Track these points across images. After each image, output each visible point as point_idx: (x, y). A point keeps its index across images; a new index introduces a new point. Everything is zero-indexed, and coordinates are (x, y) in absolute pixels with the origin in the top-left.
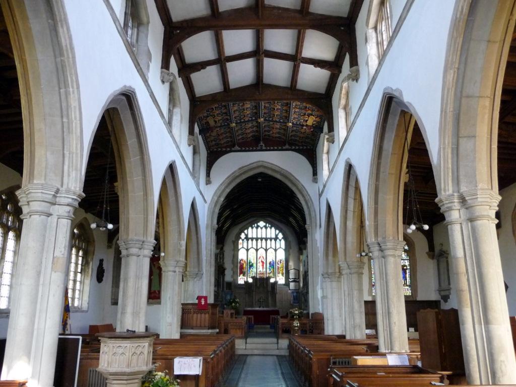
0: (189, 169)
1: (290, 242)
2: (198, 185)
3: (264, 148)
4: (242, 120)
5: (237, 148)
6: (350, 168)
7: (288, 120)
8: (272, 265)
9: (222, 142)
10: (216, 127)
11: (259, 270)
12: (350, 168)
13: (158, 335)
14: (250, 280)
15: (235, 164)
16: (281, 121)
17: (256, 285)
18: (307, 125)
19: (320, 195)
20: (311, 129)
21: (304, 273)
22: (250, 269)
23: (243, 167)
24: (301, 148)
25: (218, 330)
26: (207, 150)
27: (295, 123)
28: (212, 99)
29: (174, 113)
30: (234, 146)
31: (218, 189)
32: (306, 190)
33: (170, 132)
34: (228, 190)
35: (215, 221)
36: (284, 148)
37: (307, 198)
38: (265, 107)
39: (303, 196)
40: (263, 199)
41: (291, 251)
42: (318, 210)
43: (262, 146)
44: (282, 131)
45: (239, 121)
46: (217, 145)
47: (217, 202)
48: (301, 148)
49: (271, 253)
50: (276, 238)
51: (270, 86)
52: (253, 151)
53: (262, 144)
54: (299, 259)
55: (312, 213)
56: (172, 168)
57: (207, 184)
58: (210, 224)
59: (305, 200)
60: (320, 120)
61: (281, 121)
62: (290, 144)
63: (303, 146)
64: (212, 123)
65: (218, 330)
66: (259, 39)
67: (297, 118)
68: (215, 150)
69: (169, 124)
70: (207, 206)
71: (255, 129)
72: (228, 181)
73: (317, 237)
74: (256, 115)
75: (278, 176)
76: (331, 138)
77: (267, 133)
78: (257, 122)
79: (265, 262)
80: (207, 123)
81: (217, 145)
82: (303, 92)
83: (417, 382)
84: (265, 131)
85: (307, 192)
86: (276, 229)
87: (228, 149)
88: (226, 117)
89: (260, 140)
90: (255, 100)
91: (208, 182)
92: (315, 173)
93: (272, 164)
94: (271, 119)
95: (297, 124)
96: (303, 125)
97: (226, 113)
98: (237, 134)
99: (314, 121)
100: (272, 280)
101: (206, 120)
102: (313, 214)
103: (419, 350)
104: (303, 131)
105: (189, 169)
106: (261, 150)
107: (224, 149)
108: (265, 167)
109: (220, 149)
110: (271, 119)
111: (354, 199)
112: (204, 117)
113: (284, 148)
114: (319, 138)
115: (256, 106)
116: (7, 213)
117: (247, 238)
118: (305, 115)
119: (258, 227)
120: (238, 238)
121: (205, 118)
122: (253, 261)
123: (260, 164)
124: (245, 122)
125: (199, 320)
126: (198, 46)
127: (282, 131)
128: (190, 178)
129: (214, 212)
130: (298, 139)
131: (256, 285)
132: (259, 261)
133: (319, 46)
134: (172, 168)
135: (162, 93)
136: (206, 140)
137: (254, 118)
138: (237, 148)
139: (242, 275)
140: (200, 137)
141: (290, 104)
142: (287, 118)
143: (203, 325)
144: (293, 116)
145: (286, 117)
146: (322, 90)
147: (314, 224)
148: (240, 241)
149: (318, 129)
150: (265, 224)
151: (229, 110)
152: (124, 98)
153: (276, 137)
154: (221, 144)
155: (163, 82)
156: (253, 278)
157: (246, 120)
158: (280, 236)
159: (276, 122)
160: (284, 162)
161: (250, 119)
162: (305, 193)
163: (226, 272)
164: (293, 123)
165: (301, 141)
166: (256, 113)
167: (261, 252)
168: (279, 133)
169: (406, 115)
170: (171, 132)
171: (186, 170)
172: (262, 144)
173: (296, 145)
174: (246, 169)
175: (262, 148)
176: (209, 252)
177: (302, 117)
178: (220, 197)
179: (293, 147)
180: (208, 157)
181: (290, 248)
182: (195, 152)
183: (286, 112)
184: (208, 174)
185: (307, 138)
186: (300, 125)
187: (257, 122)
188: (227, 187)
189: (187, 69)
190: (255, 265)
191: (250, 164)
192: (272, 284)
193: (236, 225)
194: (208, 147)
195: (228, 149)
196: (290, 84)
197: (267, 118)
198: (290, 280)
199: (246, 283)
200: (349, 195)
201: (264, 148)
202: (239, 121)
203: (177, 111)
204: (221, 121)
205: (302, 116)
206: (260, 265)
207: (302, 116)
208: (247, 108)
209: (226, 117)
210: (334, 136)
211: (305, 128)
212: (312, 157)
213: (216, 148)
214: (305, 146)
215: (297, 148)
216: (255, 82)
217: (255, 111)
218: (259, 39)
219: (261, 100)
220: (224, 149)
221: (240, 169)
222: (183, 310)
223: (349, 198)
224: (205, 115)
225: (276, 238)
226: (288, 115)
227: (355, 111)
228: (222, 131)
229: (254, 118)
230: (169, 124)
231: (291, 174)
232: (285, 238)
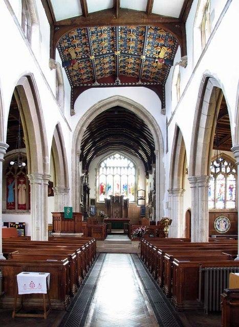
1: (139, 170)
2: (62, 112)
3: (120, 84)
4: (101, 53)
5: (97, 83)
6: (178, 130)
7: (142, 52)
8: (125, 187)
9: (84, 77)
10: (77, 59)
11: (115, 191)
12: (178, 130)
14: (109, 198)
15: (97, 98)
16: (136, 53)
17: (113, 202)
18: (159, 58)
19: (168, 124)
20: (162, 61)
21: (149, 192)
22: (108, 190)
23: (102, 101)
24: (152, 84)
25: (82, 234)
26: (71, 86)
27: (148, 55)
28: (72, 23)
29: (33, 30)
30: (94, 82)
31: (81, 119)
32: (155, 120)
34: (90, 121)
35: (79, 148)
36: (137, 84)
37: (156, 127)
38: (121, 37)
39: (153, 126)
40: (118, 131)
41: (139, 176)
42: (166, 138)
43: (118, 81)
44: (136, 66)
45: (97, 54)
46: (79, 80)
47: (80, 131)
48: (152, 84)
49: (124, 178)
50: (128, 167)
51: (126, 10)
52: (107, 86)
53: (118, 80)
54: (145, 181)
55: (160, 140)
57: (71, 115)
58: (75, 149)
59: (155, 129)
60: (171, 51)
61: (136, 53)
62: (142, 81)
63: (153, 82)
64: (74, 56)
65: (82, 234)
67: (150, 51)
68: (78, 85)
69: (57, 98)
70: (72, 134)
71: (112, 64)
72: (89, 113)
73: (165, 160)
74: (113, 47)
75: (132, 109)
76: (184, 62)
77: (122, 69)
78: (114, 55)
79: (119, 184)
80: (69, 54)
81: (79, 80)
82: (158, 17)
83: (195, 256)
84: (121, 67)
85: (156, 123)
86: (128, 159)
87: (89, 85)
88: (86, 49)
89: (116, 77)
90: (112, 24)
91: (72, 114)
92: (163, 106)
93: (127, 98)
94: (126, 52)
95: (150, 57)
96: (155, 58)
97: (85, 44)
98: (96, 69)
99: (166, 53)
100: (125, 198)
101: (68, 51)
102: (161, 140)
104: (155, 65)
106: (118, 86)
107: (85, 85)
108: (121, 101)
109: (82, 85)
110: (126, 52)
111: (208, 116)
112: (66, 47)
113: (137, 84)
114: (169, 73)
115: (113, 37)
116: (158, 229)
117: (106, 167)
118: (158, 46)
119: (114, 158)
120: (99, 166)
121: (67, 49)
122: (111, 184)
123: (116, 98)
124: (103, 54)
125: (66, 225)
127: (136, 66)
128: (53, 102)
129: (77, 139)
130: (149, 74)
131: (113, 202)
132: (115, 184)
135: (51, 75)
136: (69, 74)
137: (111, 51)
138: (97, 83)
139: (102, 194)
140: (63, 69)
141: (145, 33)
142: (141, 50)
143: (69, 229)
144: (147, 48)
145: (140, 49)
146: (176, 14)
147: (161, 150)
148: (101, 169)
149: (169, 61)
150: (119, 156)
151: (88, 40)
152: (26, 78)
153: (130, 73)
154: (83, 79)
155: (51, 69)
156: (111, 196)
157: (104, 53)
158: (132, 165)
159: (131, 54)
160: (138, 97)
161: (108, 52)
162: (154, 123)
163: (90, 191)
164: (146, 57)
165: (152, 77)
166: (113, 45)
167: (117, 178)
168: (133, 69)
169: (218, 93)
171: (50, 95)
172: (118, 80)
173: (147, 81)
174: (105, 102)
175: (118, 84)
176: (75, 172)
177: (154, 50)
178: (82, 126)
179: (145, 83)
180: (71, 91)
181: (139, 174)
183: (141, 43)
184: (72, 107)
185: (158, 73)
186: (153, 58)
187: (114, 55)
188: (88, 118)
190: (112, 187)
191: (108, 98)
192: (125, 200)
193: (97, 156)
194: (72, 83)
195: (89, 85)
196: (146, 8)
197: (123, 51)
199: (106, 200)
200: (202, 112)
201: (120, 84)
202: (97, 54)
204: (82, 53)
205: (155, 47)
206: (116, 186)
207: (155, 47)
208: (105, 39)
209: (86, 49)
210: (187, 59)
211: (157, 60)
212: (160, 89)
213: (79, 84)
214: (155, 82)
215: (149, 84)
217: (112, 43)
219: (118, 24)
220: (85, 85)
221: (99, 102)
222: (54, 217)
223: (202, 115)
224: (66, 45)
225: (128, 167)
226: (142, 47)
228: (83, 65)
229: (111, 51)
231: (143, 107)
232: (135, 167)
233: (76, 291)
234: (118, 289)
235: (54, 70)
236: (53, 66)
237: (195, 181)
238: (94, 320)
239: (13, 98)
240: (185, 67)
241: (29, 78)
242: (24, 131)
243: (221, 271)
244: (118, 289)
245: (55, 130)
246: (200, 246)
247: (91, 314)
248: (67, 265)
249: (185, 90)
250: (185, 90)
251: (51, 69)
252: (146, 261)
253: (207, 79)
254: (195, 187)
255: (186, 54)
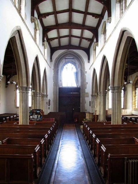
0: (31, 34)
6: (104, 58)
13: (43, 112)
33: (36, 43)
56: (37, 59)
66: (70, 32)
103: (116, 124)
105: (31, 34)
126: (53, 34)
133: (88, 34)
134: (37, 59)
135: (31, 26)
155: (32, 23)
170: (20, 12)
182: (35, 29)
189: (42, 16)
198: (33, 116)
203: (38, 32)
216: (68, 44)
218: (70, 32)
227: (128, 5)
230: (19, 10)
233: (48, 154)
234: (69, 154)
235: (33, 23)
236: (33, 21)
237: (113, 89)
238: (58, 164)
239: (9, 41)
240: (110, 23)
241: (19, 32)
242: (8, 157)
243: (133, 163)
244: (69, 154)
245: (35, 60)
246: (116, 128)
247: (56, 162)
248: (43, 143)
249: (132, 97)
250: (132, 97)
251: (32, 23)
252: (85, 136)
253: (123, 32)
254: (114, 92)
255: (111, 16)
